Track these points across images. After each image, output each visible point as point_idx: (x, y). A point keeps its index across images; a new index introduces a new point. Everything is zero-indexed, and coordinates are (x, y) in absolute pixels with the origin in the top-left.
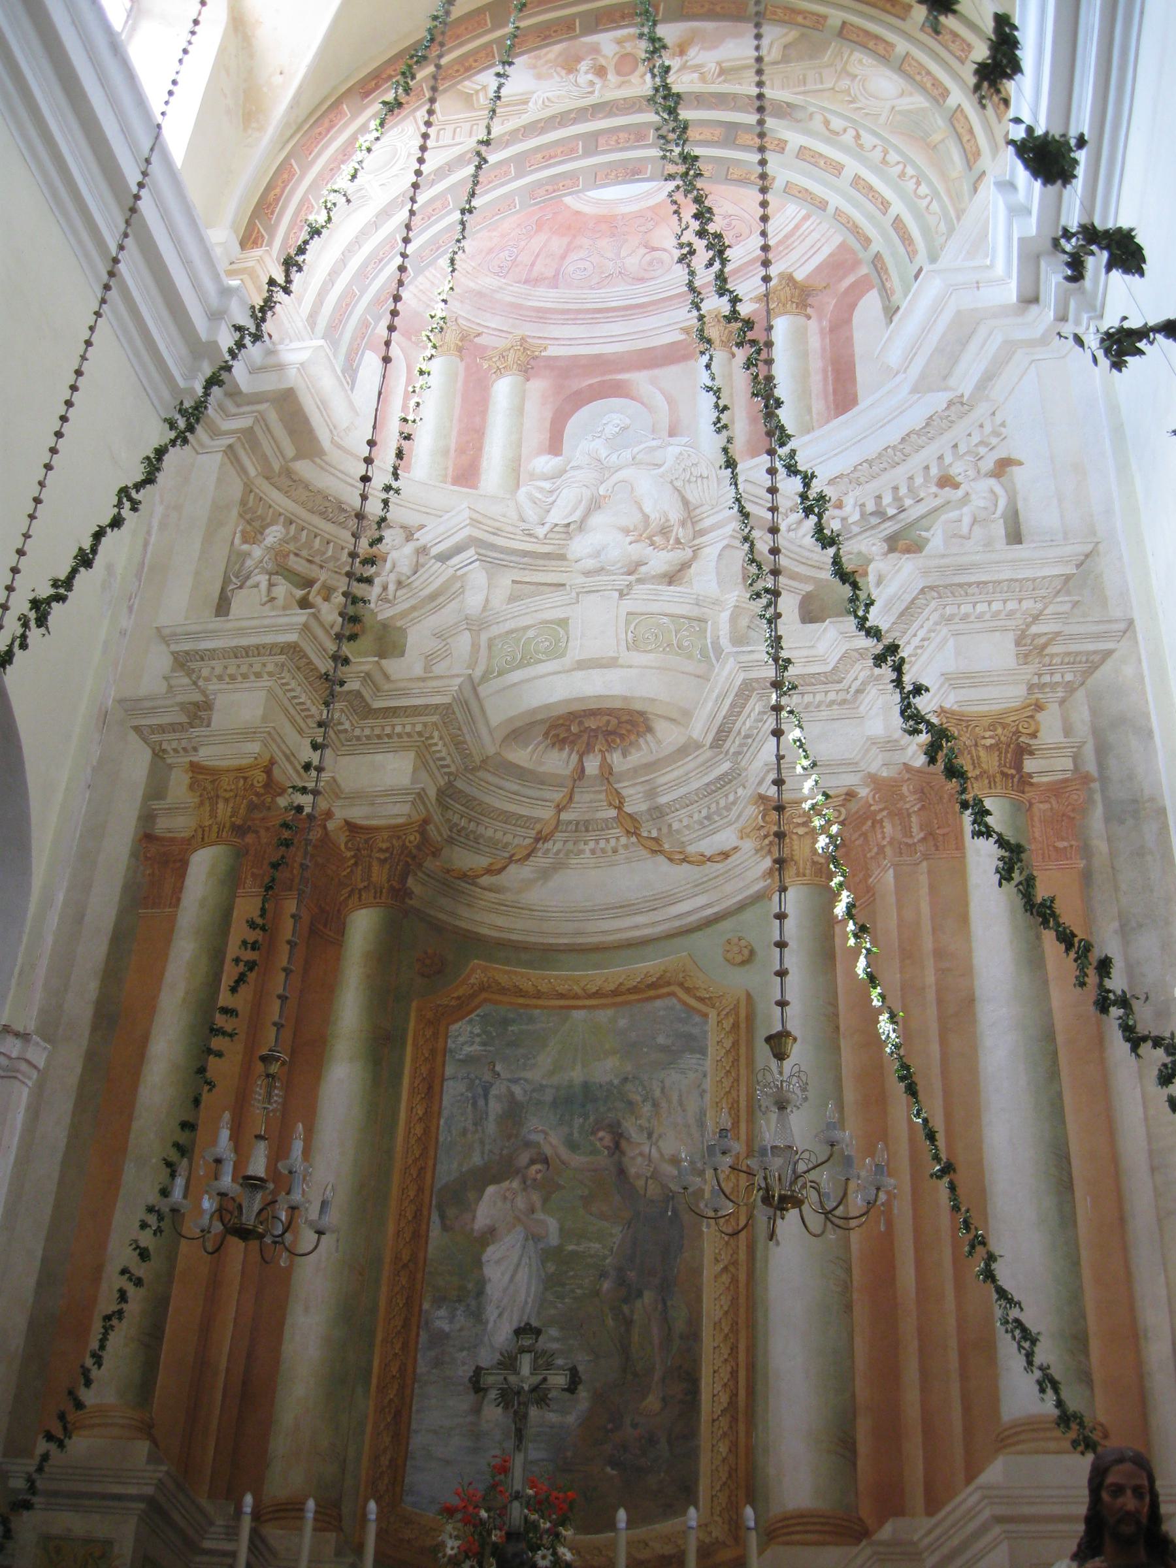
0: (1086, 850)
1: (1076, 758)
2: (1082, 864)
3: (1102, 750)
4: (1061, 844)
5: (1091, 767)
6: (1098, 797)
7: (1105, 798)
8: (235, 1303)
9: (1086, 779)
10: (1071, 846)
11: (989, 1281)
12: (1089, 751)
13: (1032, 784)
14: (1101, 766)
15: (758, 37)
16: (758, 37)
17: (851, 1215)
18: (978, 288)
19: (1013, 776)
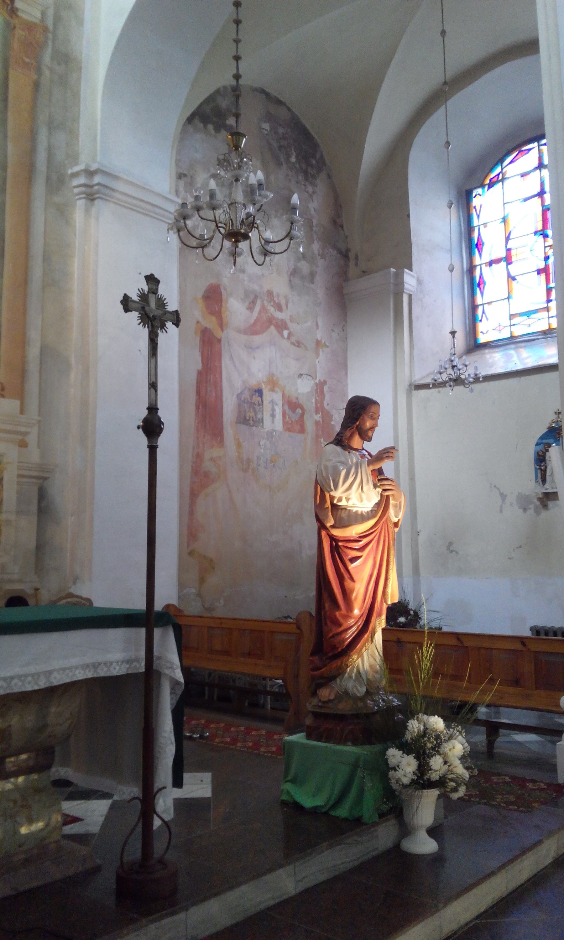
0: (39, 70)
1: (44, 14)
2: (35, 77)
3: (58, 18)
4: (27, 60)
5: (50, 23)
6: (50, 43)
7: (53, 46)
8: (10, 133)
9: (46, 30)
10: (32, 64)
11: (543, 276)
12: (50, 13)
13: (17, 16)
14: (55, 25)
15: (237, 77)
16: (237, 77)
17: (276, 252)
18: (510, 558)
19: (8, 5)
